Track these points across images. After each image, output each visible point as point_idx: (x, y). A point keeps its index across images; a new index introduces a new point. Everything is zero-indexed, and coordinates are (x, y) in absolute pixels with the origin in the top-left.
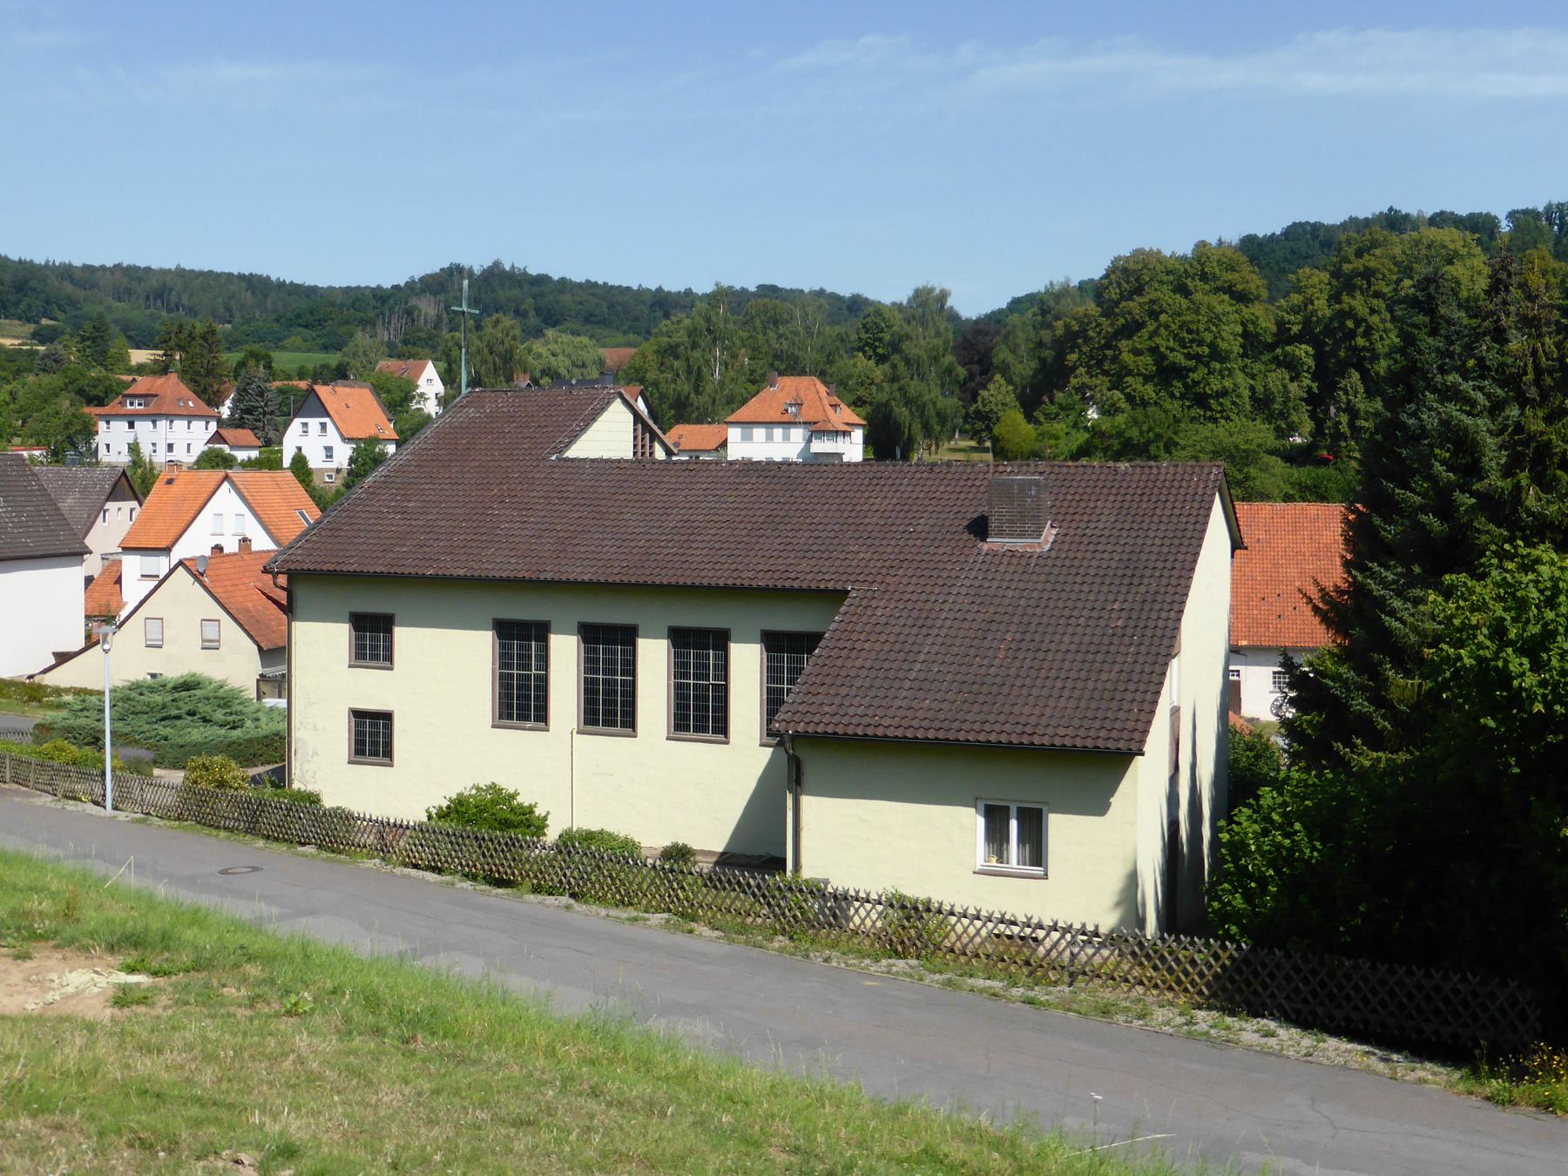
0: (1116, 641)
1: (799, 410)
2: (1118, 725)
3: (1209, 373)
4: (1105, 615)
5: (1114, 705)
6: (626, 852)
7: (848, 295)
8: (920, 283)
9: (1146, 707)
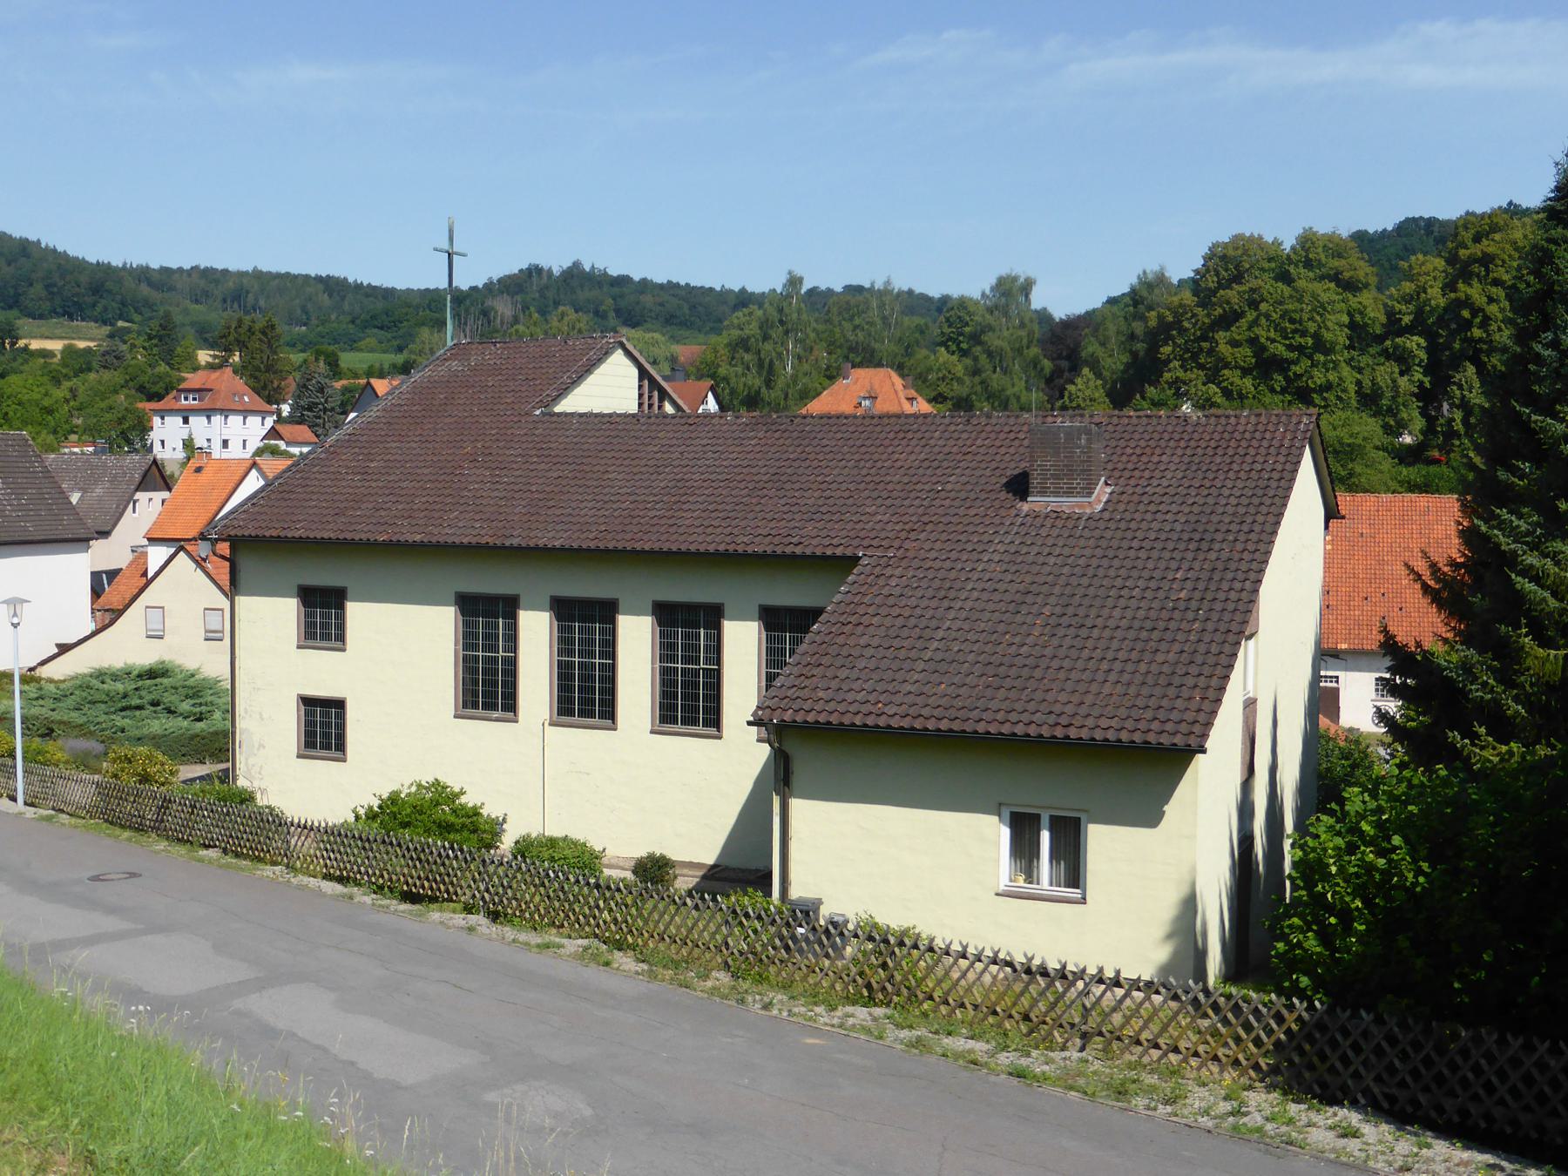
0: (1177, 615)
1: (873, 404)
2: (1175, 716)
3: (1313, 365)
4: (1166, 585)
5: (1172, 692)
6: (584, 861)
7: (937, 296)
8: (1004, 271)
9: (1211, 694)
